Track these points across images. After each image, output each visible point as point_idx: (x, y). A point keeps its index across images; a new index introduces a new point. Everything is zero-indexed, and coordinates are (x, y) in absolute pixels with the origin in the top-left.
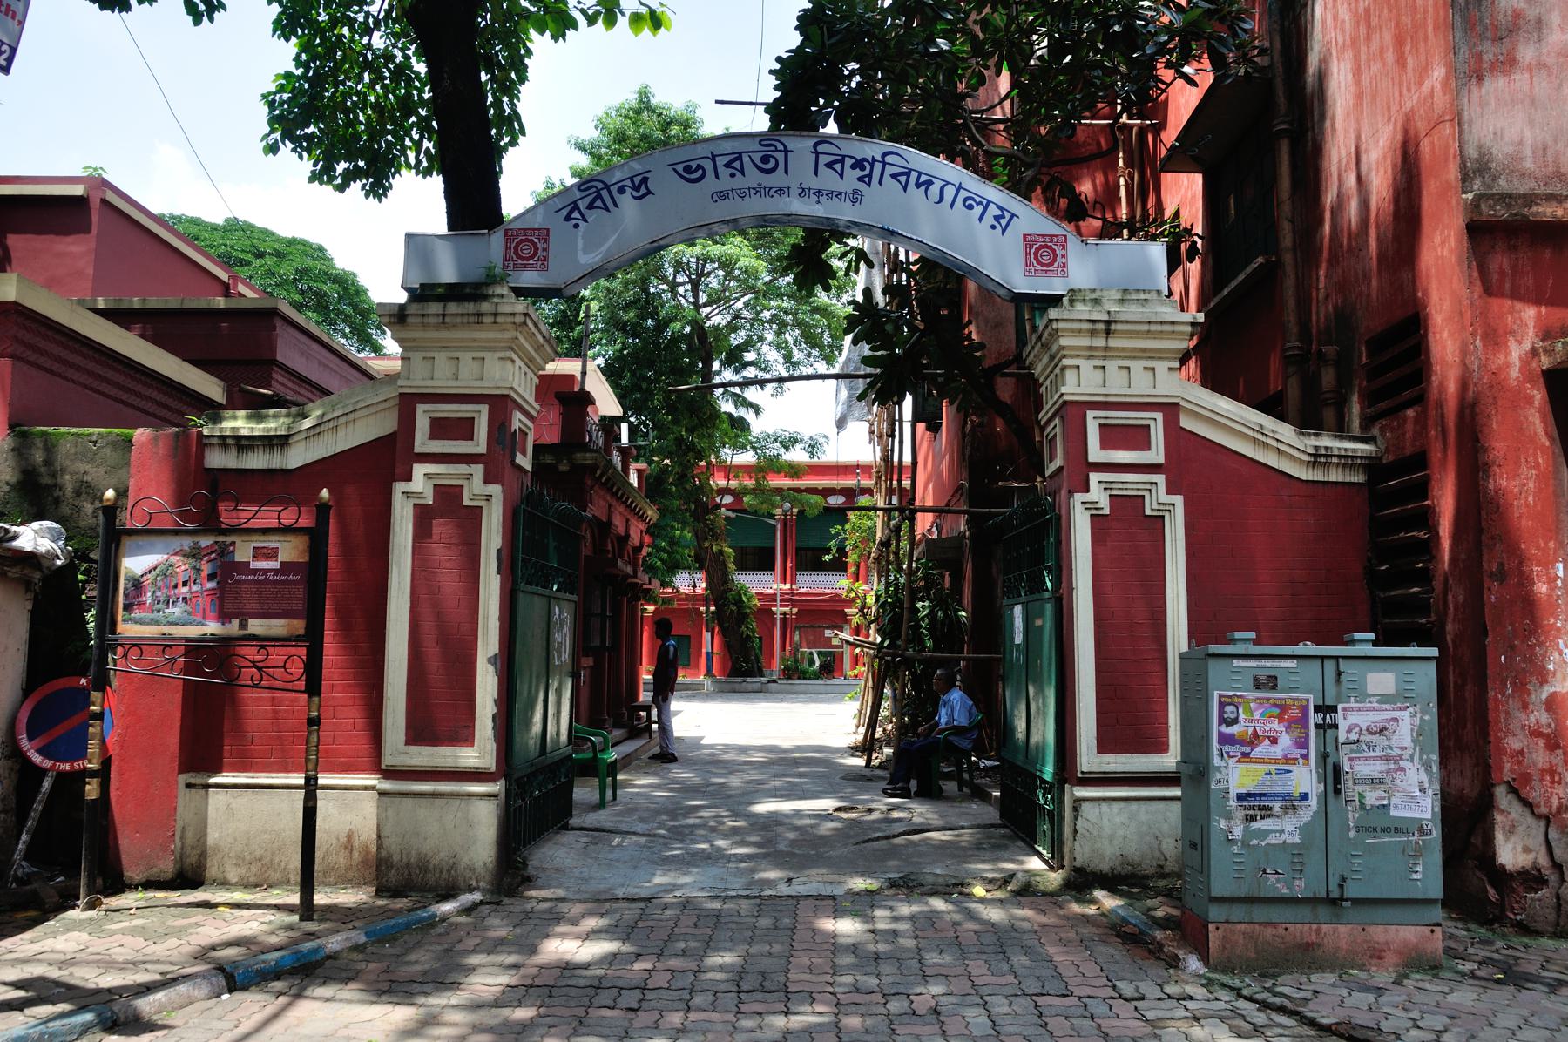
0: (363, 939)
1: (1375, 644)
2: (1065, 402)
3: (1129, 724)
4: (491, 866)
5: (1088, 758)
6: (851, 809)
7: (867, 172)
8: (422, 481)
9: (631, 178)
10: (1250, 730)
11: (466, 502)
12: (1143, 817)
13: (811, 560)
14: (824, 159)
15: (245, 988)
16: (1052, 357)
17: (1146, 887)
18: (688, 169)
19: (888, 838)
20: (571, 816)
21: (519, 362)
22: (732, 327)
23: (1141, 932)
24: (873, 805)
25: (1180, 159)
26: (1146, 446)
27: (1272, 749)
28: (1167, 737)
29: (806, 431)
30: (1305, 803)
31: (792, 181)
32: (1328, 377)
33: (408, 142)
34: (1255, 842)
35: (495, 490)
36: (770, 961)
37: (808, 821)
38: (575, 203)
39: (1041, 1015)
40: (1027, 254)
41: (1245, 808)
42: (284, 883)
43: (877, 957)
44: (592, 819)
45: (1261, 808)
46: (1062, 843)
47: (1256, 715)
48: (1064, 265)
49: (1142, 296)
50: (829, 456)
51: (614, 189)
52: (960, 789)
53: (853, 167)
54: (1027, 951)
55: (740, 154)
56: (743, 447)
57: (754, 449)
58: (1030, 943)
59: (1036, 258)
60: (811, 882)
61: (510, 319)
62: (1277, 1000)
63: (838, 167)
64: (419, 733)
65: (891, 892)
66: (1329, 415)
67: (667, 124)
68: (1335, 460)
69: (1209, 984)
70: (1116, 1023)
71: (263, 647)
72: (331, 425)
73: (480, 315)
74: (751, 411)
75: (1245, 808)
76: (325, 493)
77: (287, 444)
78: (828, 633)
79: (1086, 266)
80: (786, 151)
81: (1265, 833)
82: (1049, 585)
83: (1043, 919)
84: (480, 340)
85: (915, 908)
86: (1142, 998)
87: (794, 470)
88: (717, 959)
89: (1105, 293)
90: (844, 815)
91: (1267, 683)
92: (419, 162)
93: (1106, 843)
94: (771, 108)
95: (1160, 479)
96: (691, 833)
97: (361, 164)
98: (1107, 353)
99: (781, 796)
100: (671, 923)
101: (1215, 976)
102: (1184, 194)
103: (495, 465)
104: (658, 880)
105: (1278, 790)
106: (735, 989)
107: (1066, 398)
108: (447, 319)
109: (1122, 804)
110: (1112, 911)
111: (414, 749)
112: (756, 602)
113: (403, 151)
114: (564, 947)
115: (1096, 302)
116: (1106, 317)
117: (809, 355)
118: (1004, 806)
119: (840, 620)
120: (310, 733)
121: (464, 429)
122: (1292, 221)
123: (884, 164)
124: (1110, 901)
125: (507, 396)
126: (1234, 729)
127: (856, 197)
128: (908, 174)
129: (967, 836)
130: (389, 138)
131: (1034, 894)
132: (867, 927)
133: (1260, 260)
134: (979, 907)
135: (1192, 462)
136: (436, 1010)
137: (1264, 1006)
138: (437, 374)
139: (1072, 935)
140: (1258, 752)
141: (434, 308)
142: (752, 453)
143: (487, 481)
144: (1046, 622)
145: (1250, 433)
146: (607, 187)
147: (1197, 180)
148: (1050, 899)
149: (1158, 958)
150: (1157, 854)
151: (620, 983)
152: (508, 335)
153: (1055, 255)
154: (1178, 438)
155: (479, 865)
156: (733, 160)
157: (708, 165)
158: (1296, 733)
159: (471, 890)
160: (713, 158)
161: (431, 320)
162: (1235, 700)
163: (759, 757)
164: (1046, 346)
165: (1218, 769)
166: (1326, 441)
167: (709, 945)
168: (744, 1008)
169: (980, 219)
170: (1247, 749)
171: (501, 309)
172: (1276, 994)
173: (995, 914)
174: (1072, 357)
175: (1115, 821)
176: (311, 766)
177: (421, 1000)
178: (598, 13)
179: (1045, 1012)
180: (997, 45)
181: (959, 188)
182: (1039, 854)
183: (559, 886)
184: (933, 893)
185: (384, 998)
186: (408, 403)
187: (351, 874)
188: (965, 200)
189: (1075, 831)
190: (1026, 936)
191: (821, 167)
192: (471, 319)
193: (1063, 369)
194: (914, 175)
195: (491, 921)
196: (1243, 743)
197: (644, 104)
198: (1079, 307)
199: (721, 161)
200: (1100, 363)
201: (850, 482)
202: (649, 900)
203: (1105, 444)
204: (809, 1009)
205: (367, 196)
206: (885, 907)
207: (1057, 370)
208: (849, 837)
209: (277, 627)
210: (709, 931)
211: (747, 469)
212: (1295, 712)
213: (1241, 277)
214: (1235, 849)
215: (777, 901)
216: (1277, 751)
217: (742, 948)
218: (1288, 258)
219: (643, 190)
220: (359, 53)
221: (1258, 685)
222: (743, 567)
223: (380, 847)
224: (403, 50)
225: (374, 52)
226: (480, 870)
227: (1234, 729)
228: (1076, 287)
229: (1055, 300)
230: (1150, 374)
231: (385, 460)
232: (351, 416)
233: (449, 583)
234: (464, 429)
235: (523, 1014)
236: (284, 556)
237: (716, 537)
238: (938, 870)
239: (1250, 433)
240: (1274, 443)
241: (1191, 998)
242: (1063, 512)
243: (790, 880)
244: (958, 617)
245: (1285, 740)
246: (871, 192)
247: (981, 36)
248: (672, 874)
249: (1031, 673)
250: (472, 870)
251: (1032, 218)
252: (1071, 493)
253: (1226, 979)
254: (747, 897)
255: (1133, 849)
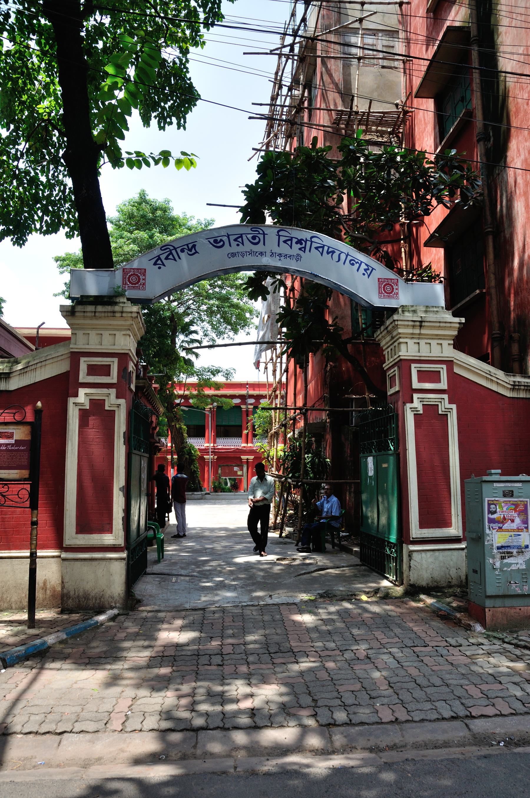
0: (65, 637)
1: (501, 475)
2: (401, 360)
3: (434, 513)
4: (122, 595)
5: (415, 530)
6: (284, 559)
7: (303, 246)
8: (83, 397)
9: (187, 245)
10: (502, 516)
11: (107, 408)
12: (441, 558)
13: (234, 431)
14: (282, 239)
15: (12, 666)
16: (393, 338)
17: (444, 593)
18: (216, 241)
19: (309, 573)
20: (147, 567)
21: (132, 337)
22: (186, 314)
23: (449, 614)
24: (295, 557)
25: (431, 242)
26: (439, 381)
27: (512, 525)
28: (451, 520)
29: (224, 367)
30: (527, 549)
31: (267, 249)
32: (515, 348)
33: (36, 218)
34: (505, 569)
35: (122, 402)
36: (278, 637)
37: (266, 566)
38: (159, 256)
39: (418, 656)
40: (380, 288)
41: (501, 553)
42: (21, 609)
43: (329, 632)
44: (157, 568)
45: (508, 553)
46: (402, 573)
47: (505, 509)
48: (397, 294)
49: (435, 309)
50: (237, 378)
51: (179, 250)
52: (333, 547)
53: (297, 243)
54: (399, 626)
55: (242, 234)
56: (193, 374)
57: (197, 375)
58: (399, 622)
59: (384, 290)
60: (280, 597)
61: (130, 315)
62: (522, 643)
63: (289, 242)
64: (83, 527)
65: (322, 600)
66: (516, 366)
67: (154, 210)
68: (523, 387)
69: (488, 637)
70: (454, 658)
71: (6, 484)
72: (33, 367)
73: (114, 312)
74: (194, 356)
75: (501, 553)
76: (39, 404)
77: (9, 377)
78: (236, 469)
79: (406, 295)
80: (264, 234)
81: (510, 564)
82: (392, 448)
83: (399, 610)
84: (114, 325)
85: (337, 608)
86: (461, 646)
87: (218, 386)
88: (250, 638)
89: (418, 308)
90: (283, 562)
91: (509, 494)
92: (42, 227)
93: (424, 572)
94: (243, 209)
95: (446, 396)
96: (210, 574)
97: (11, 227)
98: (420, 336)
99: (243, 554)
100: (221, 620)
101: (490, 633)
102: (435, 258)
103: (121, 390)
104: (203, 599)
105: (515, 544)
106: (267, 652)
107: (401, 357)
108: (97, 314)
109: (431, 553)
110: (431, 604)
111: (80, 536)
112: (199, 453)
113: (34, 221)
114: (172, 635)
115: (414, 312)
116: (420, 319)
117: (226, 328)
118: (362, 556)
119: (240, 463)
120: (32, 529)
121: (105, 370)
122: (494, 274)
123: (312, 242)
124: (430, 601)
125: (127, 354)
126: (495, 516)
127: (298, 258)
128: (323, 247)
129: (347, 571)
130: (26, 215)
131: (391, 598)
132: (317, 618)
133: (478, 291)
134: (364, 605)
135: (461, 389)
136: (118, 672)
137: (517, 646)
138: (91, 342)
139: (416, 617)
140: (506, 526)
141: (90, 308)
142: (196, 377)
143: (118, 397)
144: (390, 465)
145: (485, 374)
146: (175, 249)
147: (442, 251)
148: (399, 600)
149: (460, 626)
150: (448, 576)
151: (209, 652)
152: (129, 323)
153: (393, 289)
154: (453, 377)
155: (116, 595)
156: (238, 238)
157: (225, 239)
158: (522, 517)
159: (112, 608)
160: (228, 236)
161: (89, 314)
162: (495, 502)
163: (222, 533)
164: (389, 332)
165: (488, 535)
166: (518, 379)
167: (244, 631)
168: (275, 661)
169: (358, 270)
170: (500, 525)
171: (125, 310)
172: (520, 640)
173: (376, 609)
174: (404, 338)
175: (426, 562)
176: (33, 547)
177: (109, 667)
178: (160, 159)
179: (419, 654)
180: (349, 183)
181: (347, 255)
182: (387, 578)
183: (155, 604)
184: (343, 600)
185: (88, 667)
186: (75, 357)
187: (45, 602)
188: (351, 261)
189: (410, 567)
190: (396, 619)
191: (281, 243)
192: (109, 314)
193: (399, 343)
194: (326, 248)
195: (126, 624)
196: (499, 522)
197: (143, 199)
198: (407, 314)
199: (232, 238)
200: (417, 341)
201: (244, 392)
202: (203, 609)
203: (420, 380)
204: (308, 660)
205: (14, 244)
206: (323, 608)
207: (396, 344)
208: (290, 573)
209: (13, 474)
210: (241, 624)
211: (193, 385)
212: (521, 507)
213: (468, 299)
214: (497, 573)
215: (268, 607)
216: (514, 526)
217: (262, 632)
218: (493, 291)
219: (193, 251)
220: (12, 170)
221: (505, 496)
222: (191, 435)
223: (63, 588)
224: (34, 169)
225: (19, 170)
226: (117, 598)
227: (495, 516)
228: (404, 304)
229: (394, 310)
230: (440, 346)
231: (62, 387)
232: (43, 363)
233: (97, 449)
234: (105, 370)
235: (164, 671)
236: (16, 437)
237: (178, 420)
238: (341, 588)
239: (485, 374)
240: (495, 380)
241: (483, 644)
242: (400, 412)
243: (270, 596)
244: (326, 462)
245: (518, 520)
246: (305, 256)
247: (342, 178)
248: (210, 595)
249: (380, 489)
250: (112, 597)
251: (381, 271)
252: (404, 403)
253: (495, 634)
254: (252, 605)
255: (437, 575)
